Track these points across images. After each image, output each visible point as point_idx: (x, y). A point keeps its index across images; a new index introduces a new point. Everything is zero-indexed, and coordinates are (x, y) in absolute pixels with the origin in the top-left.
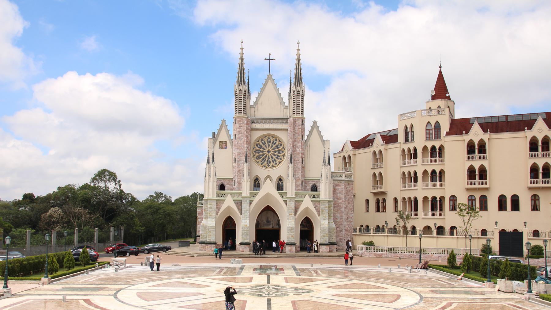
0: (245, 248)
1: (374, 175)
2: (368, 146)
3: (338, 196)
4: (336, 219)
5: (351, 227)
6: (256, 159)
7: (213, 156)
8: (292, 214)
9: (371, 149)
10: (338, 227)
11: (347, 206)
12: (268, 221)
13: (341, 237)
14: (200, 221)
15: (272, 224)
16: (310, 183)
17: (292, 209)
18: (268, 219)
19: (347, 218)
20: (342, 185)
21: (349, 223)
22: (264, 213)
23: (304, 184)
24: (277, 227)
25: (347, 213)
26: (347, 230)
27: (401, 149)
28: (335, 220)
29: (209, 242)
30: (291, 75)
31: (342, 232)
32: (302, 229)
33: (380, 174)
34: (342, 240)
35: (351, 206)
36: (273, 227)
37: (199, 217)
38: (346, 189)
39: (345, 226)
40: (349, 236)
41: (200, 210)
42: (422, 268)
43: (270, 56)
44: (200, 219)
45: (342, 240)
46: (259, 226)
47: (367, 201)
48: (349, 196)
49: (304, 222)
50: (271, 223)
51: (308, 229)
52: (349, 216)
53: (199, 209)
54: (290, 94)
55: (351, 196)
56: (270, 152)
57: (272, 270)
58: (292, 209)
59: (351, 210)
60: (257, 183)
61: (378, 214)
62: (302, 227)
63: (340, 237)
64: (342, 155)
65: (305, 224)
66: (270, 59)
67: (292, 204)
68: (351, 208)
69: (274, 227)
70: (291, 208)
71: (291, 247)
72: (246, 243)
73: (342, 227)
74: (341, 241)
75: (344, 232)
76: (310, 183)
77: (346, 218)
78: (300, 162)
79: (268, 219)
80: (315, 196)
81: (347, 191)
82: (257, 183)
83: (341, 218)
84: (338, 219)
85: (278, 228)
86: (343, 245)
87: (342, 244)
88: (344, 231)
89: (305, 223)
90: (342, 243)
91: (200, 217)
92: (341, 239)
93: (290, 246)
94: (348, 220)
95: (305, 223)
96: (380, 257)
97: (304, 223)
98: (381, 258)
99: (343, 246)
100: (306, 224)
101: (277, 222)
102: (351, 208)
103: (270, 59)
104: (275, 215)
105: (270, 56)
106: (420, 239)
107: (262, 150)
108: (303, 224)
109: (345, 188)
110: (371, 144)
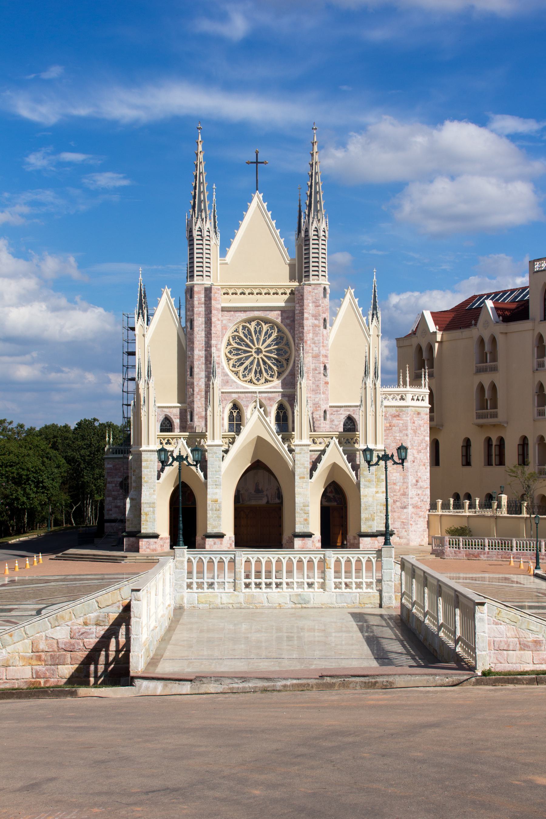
0: (215, 544)
1: (481, 388)
2: (468, 325)
3: (397, 438)
4: (394, 484)
5: (424, 500)
6: (233, 367)
7: (149, 367)
8: (303, 478)
9: (474, 333)
10: (397, 501)
11: (415, 458)
12: (258, 491)
13: (404, 521)
14: (110, 488)
15: (267, 495)
16: (341, 414)
17: (305, 468)
18: (257, 485)
19: (417, 481)
20: (404, 416)
21: (420, 492)
22: (251, 473)
23: (328, 416)
24: (277, 501)
25: (417, 472)
26: (416, 507)
27: (536, 334)
28: (392, 486)
29: (153, 533)
30: (300, 195)
31: (405, 510)
32: (326, 504)
33: (494, 387)
34: (406, 526)
35: (425, 457)
36: (268, 502)
37: (109, 480)
38: (414, 423)
39: (411, 498)
40: (420, 517)
41: (111, 466)
42: (425, 574)
43: (257, 155)
44: (111, 485)
45: (406, 526)
46: (241, 500)
47: (467, 444)
48: (421, 438)
49: (329, 490)
50: (265, 493)
51: (337, 504)
52: (420, 478)
53: (108, 464)
54: (298, 235)
55: (424, 436)
56: (258, 355)
57: (222, 307)
58: (305, 468)
59: (424, 465)
60: (235, 414)
61: (489, 468)
62: (326, 501)
63: (401, 520)
64: (415, 341)
65: (331, 495)
66: (257, 163)
67: (304, 457)
68: (424, 461)
69: (270, 502)
70: (303, 464)
71: (304, 540)
72: (217, 534)
73: (405, 500)
74: (404, 528)
75: (410, 509)
76: (341, 414)
77: (414, 481)
78: (319, 373)
79: (257, 485)
80: (350, 440)
81: (415, 428)
82: (235, 414)
83: (404, 482)
84: (398, 484)
85: (278, 503)
86: (408, 535)
87: (406, 533)
88: (410, 507)
89: (331, 492)
90: (406, 531)
91: (112, 480)
92: (404, 525)
93: (301, 539)
94: (418, 486)
95: (331, 492)
96: (476, 560)
97: (330, 492)
98: (479, 560)
99: (408, 537)
100: (333, 494)
101: (277, 492)
102: (424, 461)
103: (257, 163)
104: (272, 477)
105: (257, 155)
106: (537, 524)
107: (244, 355)
108: (328, 494)
109: (412, 421)
110: (473, 322)
